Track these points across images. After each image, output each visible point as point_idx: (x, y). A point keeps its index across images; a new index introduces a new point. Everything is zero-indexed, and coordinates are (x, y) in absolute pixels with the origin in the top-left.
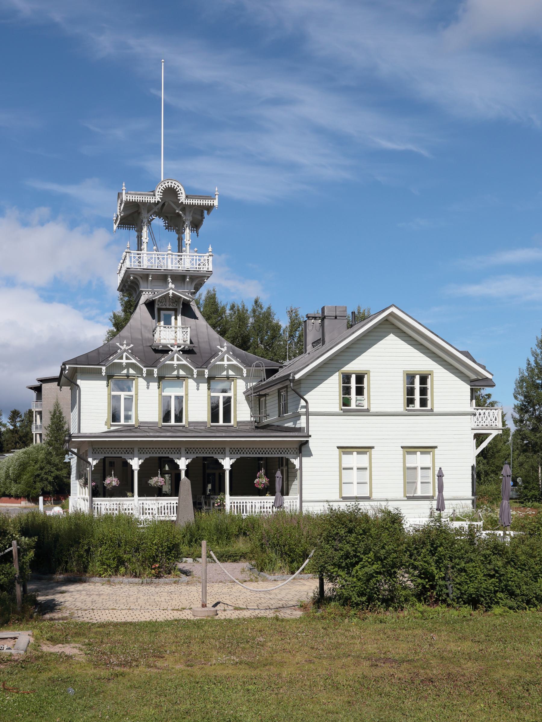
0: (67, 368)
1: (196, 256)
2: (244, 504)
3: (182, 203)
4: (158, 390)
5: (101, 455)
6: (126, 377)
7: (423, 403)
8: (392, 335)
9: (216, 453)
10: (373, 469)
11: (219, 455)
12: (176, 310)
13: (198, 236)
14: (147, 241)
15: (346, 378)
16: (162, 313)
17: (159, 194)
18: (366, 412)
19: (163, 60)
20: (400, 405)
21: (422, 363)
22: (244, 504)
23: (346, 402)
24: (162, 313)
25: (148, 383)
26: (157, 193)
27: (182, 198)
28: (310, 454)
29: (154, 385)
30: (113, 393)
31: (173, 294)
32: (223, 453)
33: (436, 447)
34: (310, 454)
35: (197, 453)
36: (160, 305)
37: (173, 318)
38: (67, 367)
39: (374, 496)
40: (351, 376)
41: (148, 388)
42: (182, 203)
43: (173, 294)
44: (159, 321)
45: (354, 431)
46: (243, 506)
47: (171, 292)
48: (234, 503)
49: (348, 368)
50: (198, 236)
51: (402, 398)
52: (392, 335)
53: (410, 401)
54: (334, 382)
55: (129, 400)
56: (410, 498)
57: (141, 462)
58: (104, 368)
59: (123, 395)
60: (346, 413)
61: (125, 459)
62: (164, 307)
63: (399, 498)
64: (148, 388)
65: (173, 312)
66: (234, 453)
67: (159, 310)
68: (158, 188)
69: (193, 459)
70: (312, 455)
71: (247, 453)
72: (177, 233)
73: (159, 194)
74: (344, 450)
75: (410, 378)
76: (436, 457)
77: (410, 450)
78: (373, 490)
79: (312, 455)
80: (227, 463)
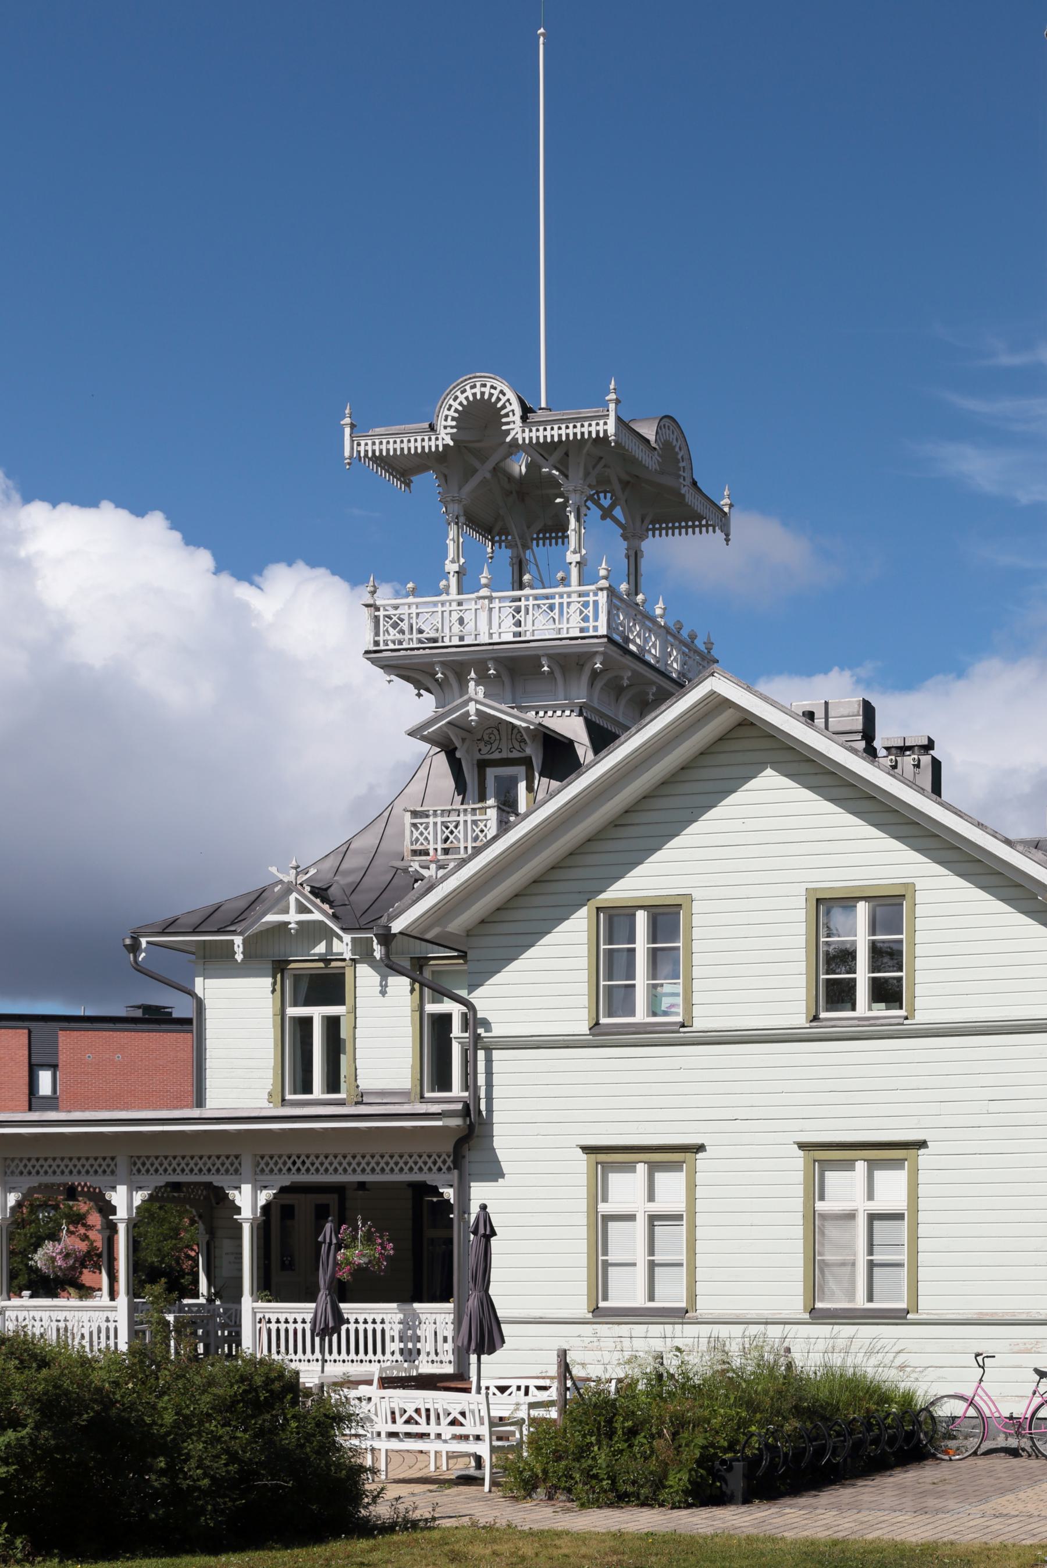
0: (144, 945)
1: (561, 596)
2: (379, 1327)
3: (453, 437)
4: (409, 997)
5: (155, 1177)
6: (322, 965)
7: (887, 993)
8: (769, 771)
9: (218, 1170)
10: (700, 1219)
11: (228, 1177)
12: (527, 762)
13: (727, 540)
14: (577, 558)
15: (616, 922)
16: (491, 773)
17: (450, 423)
18: (679, 1034)
19: (542, 30)
20: (790, 998)
21: (877, 859)
22: (379, 1327)
23: (618, 999)
24: (491, 773)
25: (384, 978)
26: (441, 423)
27: (516, 429)
28: (494, 1172)
29: (400, 985)
30: (431, 1008)
31: (478, 712)
32: (110, 1172)
33: (922, 1144)
34: (494, 1172)
35: (165, 1170)
36: (485, 750)
37: (522, 786)
38: (143, 941)
39: (705, 1306)
40: (633, 916)
41: (383, 993)
42: (515, 439)
43: (478, 712)
44: (482, 798)
45: (638, 1092)
46: (374, 1331)
47: (472, 707)
48: (295, 1322)
49: (625, 889)
50: (727, 540)
51: (801, 981)
52: (769, 771)
53: (840, 994)
54: (571, 940)
55: (332, 1024)
56: (817, 1316)
57: (139, 1198)
58: (238, 940)
59: (317, 1013)
60: (600, 1035)
61: (222, 1188)
62: (496, 756)
63: (785, 1315)
64: (383, 993)
65: (521, 770)
66: (148, 1171)
67: (482, 765)
68: (442, 416)
69: (283, 1190)
70: (502, 1175)
71: (411, 1169)
72: (625, 537)
73: (450, 423)
74: (602, 1157)
75: (826, 906)
76: (922, 1177)
77: (825, 1155)
78: (700, 1288)
79: (502, 1175)
80: (248, 1201)
